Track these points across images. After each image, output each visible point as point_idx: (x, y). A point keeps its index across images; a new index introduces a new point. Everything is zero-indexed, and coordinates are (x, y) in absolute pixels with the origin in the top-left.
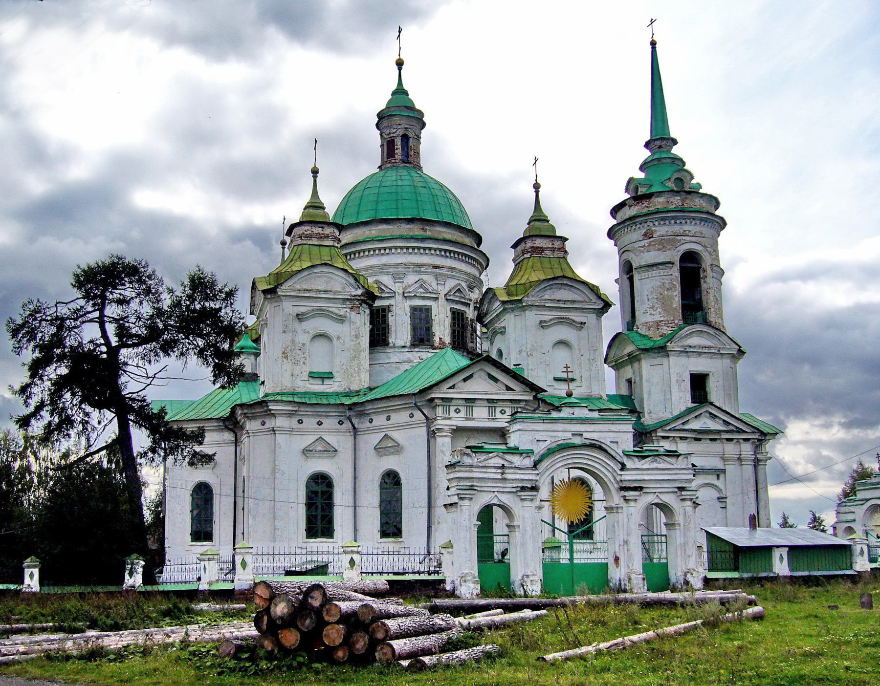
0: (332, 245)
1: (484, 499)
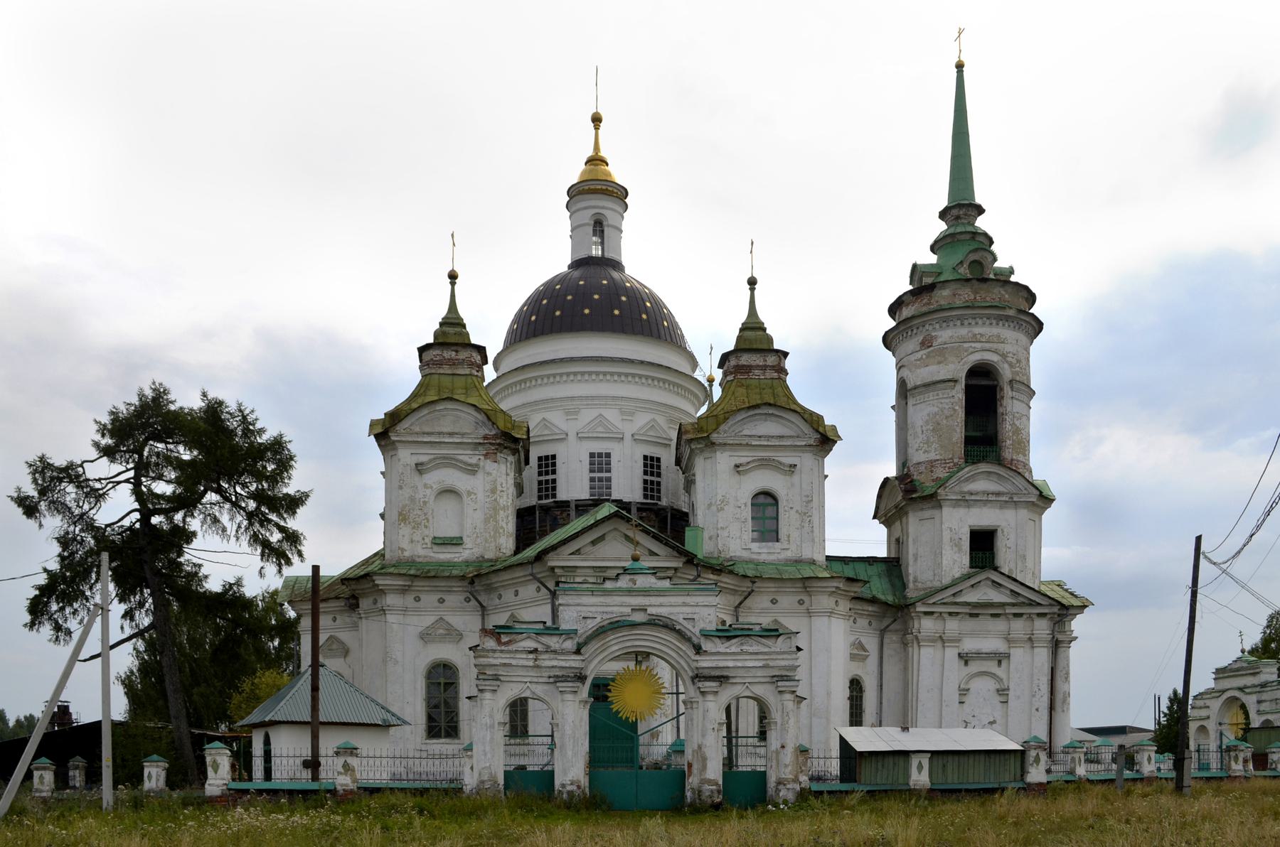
0: (468, 373)
1: (510, 692)
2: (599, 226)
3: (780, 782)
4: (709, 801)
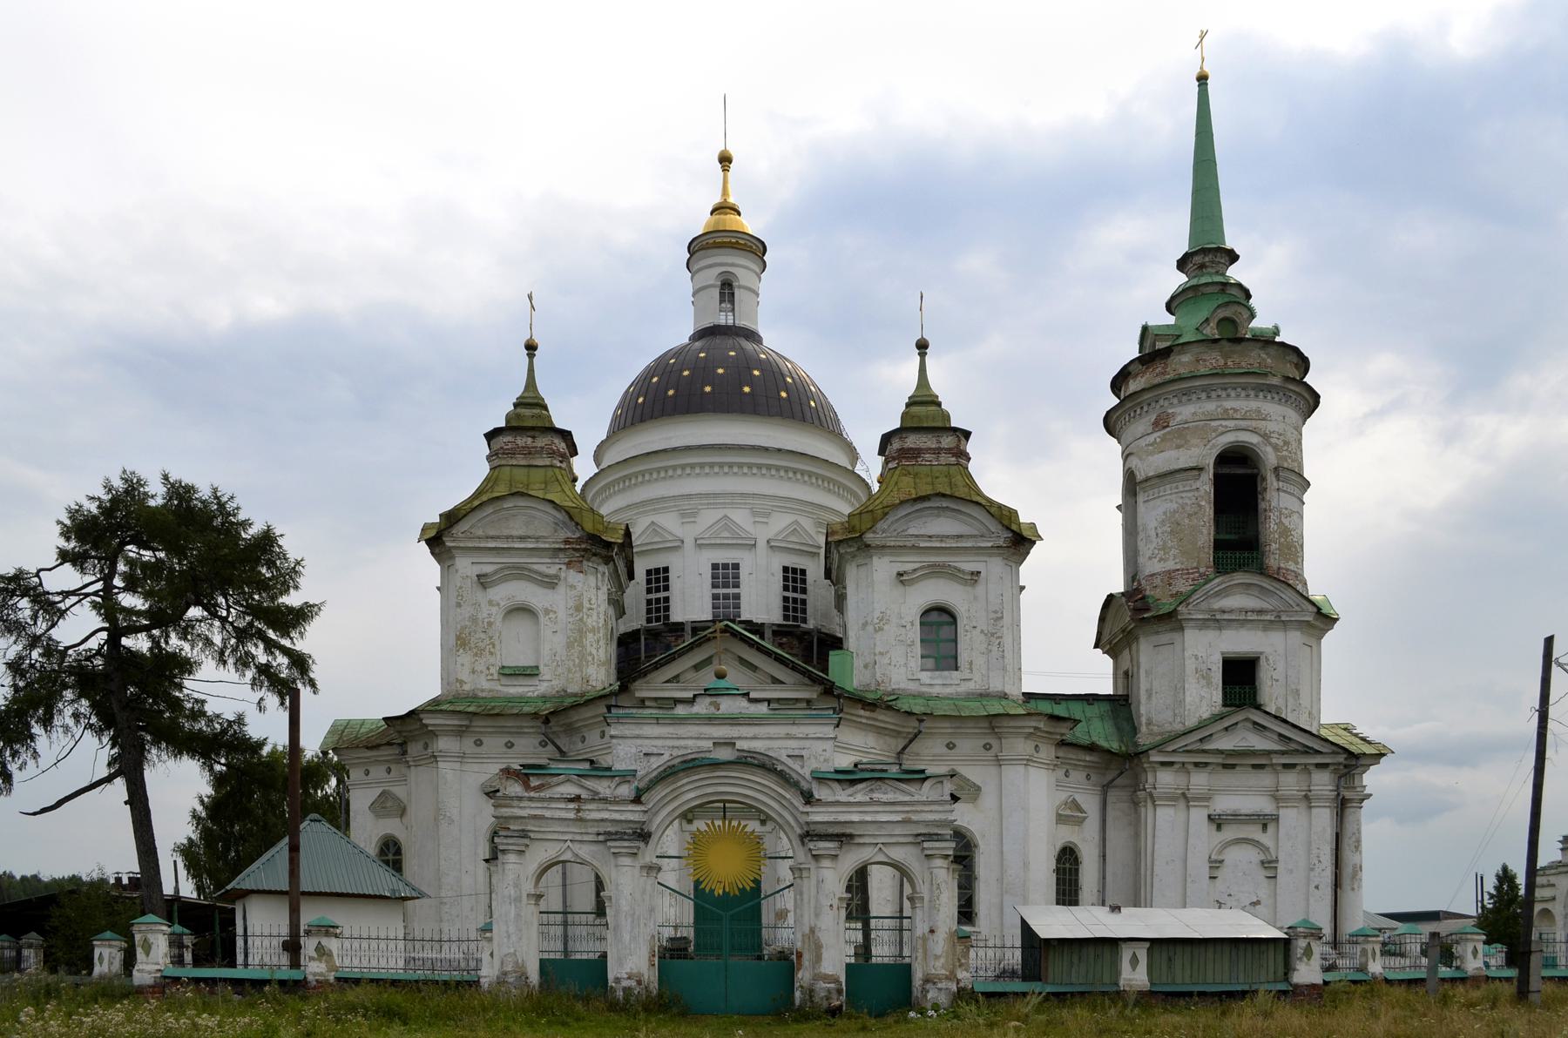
0: (548, 463)
2: (727, 289)
3: (927, 980)
4: (825, 1004)
